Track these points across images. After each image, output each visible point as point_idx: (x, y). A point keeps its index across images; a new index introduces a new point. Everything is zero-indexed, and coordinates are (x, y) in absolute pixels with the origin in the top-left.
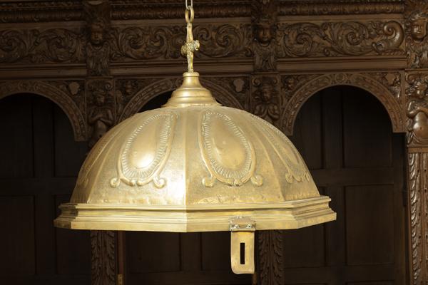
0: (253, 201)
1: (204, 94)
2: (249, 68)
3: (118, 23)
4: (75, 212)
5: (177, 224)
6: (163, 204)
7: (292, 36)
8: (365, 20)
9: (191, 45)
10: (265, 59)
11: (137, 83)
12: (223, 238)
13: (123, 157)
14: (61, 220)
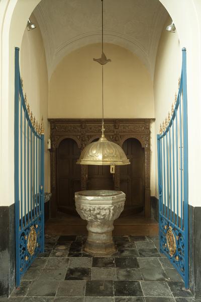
0: (115, 160)
1: (105, 139)
2: (113, 134)
3: (87, 124)
4: (81, 161)
5: (100, 163)
6: (98, 160)
7: (122, 127)
8: (137, 125)
9: (103, 130)
10: (117, 132)
11: (91, 136)
12: (109, 167)
13: (90, 151)
14: (78, 163)
